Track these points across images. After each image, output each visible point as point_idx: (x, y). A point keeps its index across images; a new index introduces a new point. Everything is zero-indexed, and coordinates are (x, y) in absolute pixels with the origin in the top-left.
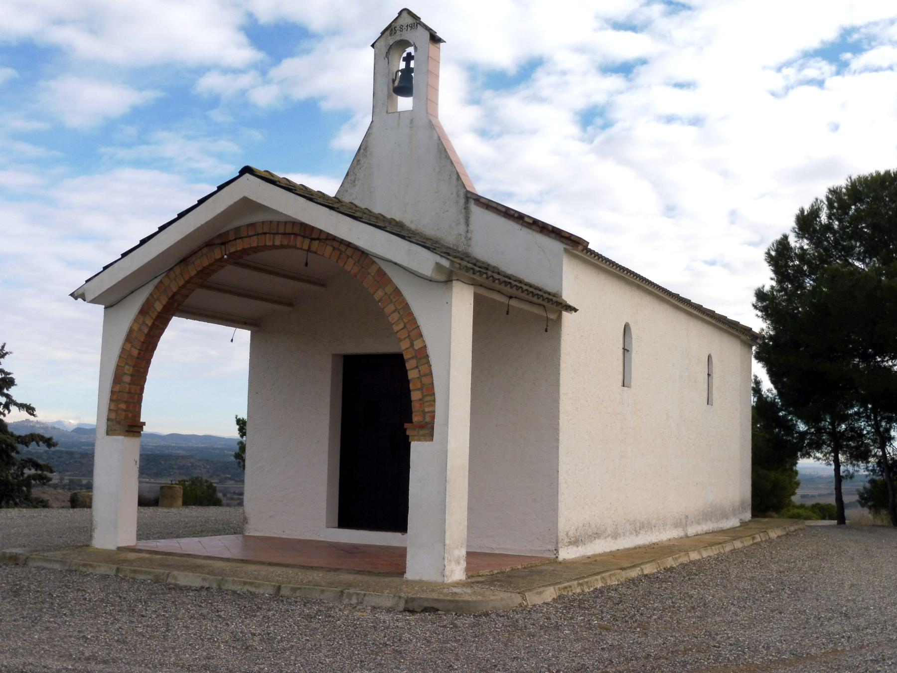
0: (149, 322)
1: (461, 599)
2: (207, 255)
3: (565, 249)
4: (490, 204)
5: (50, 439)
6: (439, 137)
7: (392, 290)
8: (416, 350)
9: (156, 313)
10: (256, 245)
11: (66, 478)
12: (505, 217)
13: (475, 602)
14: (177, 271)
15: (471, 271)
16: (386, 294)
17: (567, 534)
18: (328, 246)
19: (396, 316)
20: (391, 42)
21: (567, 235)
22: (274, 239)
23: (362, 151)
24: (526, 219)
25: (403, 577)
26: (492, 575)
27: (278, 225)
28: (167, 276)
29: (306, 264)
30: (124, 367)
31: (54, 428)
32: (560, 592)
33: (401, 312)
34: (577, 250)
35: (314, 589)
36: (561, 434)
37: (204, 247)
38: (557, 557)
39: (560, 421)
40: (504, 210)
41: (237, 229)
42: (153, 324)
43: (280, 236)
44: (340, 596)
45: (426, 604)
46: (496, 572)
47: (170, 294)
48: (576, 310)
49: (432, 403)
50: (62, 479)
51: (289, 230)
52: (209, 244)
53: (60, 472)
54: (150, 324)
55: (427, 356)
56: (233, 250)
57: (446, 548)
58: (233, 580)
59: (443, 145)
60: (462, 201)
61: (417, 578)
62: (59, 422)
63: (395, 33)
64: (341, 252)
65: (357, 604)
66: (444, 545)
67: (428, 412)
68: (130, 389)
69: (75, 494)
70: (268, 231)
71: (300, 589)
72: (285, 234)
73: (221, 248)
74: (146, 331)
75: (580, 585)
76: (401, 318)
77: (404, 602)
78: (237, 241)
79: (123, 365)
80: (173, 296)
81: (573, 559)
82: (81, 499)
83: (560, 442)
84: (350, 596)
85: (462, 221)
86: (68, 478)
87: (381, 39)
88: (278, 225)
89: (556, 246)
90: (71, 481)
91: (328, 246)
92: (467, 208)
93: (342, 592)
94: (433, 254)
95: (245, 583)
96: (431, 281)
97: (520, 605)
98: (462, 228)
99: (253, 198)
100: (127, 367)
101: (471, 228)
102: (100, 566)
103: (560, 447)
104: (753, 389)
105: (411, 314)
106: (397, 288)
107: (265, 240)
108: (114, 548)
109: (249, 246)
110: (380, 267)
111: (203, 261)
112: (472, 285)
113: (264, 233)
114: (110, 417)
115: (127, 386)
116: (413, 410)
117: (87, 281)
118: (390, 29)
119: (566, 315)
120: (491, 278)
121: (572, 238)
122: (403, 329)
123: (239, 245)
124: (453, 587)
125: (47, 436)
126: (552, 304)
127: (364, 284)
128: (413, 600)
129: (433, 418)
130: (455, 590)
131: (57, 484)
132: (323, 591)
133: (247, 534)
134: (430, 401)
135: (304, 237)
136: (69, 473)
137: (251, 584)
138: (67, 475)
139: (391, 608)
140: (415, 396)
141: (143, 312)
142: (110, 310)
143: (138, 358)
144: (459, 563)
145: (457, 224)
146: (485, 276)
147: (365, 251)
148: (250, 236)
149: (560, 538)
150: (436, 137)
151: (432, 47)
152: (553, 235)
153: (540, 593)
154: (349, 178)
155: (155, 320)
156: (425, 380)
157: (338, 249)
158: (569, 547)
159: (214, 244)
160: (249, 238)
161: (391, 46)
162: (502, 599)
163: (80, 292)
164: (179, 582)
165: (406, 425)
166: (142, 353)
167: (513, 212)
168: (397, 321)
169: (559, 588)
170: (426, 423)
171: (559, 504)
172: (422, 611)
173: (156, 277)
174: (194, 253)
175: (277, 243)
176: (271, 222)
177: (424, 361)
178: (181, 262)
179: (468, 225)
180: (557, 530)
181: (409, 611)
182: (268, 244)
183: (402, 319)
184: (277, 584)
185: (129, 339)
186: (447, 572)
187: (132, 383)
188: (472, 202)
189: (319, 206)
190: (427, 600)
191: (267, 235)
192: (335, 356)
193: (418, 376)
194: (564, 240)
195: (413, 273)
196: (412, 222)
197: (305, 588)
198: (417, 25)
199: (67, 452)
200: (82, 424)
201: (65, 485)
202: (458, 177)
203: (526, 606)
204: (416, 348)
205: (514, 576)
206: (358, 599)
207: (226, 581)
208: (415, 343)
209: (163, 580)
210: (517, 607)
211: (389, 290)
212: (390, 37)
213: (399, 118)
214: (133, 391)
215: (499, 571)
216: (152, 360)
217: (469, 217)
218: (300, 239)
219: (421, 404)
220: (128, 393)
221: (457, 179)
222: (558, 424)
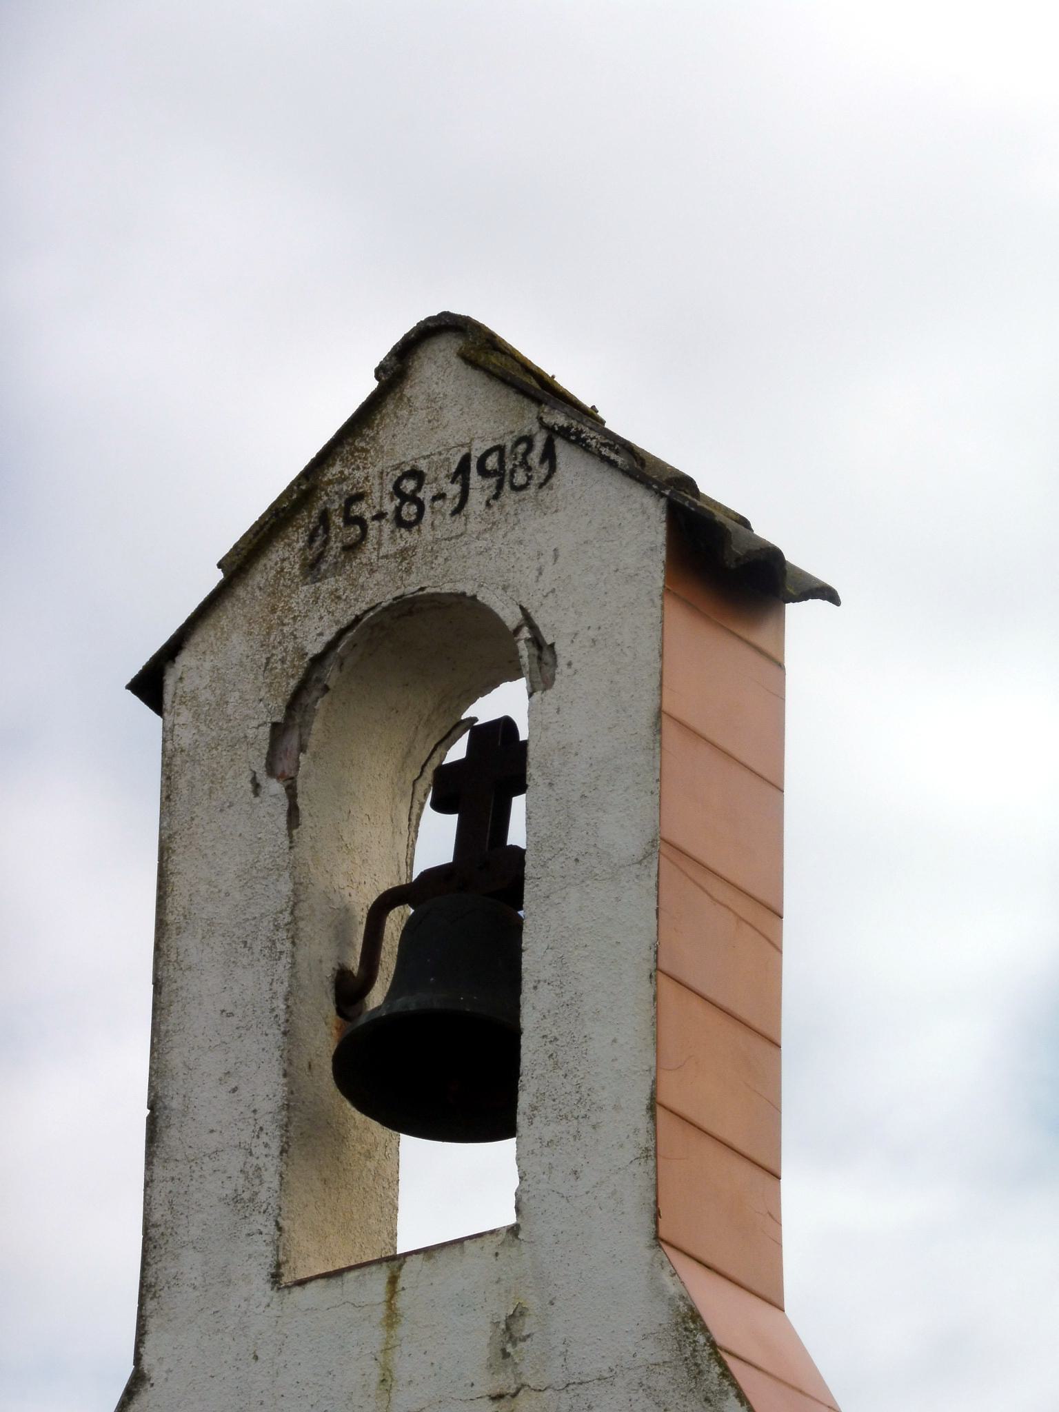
63: (351, 549)
87: (231, 614)
104: (342, 975)
161: (318, 660)
195: (758, 901)
198: (549, 455)
212: (305, 590)
213: (392, 1317)
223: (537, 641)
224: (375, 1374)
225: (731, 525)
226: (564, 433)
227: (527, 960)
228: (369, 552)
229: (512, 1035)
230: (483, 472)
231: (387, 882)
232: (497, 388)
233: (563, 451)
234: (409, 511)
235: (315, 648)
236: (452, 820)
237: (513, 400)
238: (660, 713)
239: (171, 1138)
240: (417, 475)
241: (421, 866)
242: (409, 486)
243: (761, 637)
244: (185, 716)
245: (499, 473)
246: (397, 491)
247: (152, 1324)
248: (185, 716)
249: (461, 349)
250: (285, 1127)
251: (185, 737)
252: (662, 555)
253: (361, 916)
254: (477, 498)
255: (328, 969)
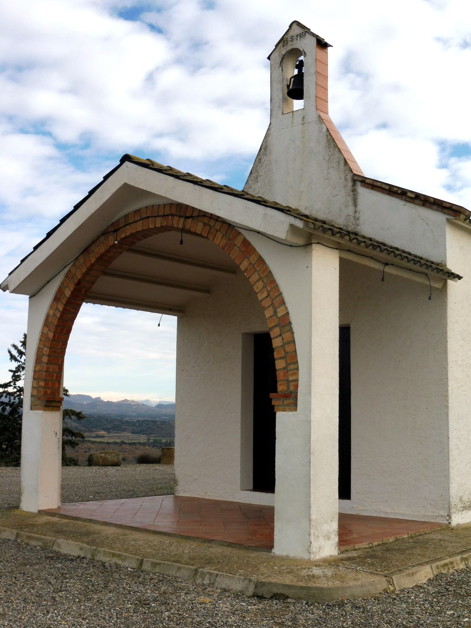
0: (61, 308)
1: (314, 585)
2: (103, 243)
3: (447, 219)
4: (375, 183)
5: (80, 413)
6: (327, 129)
7: (256, 259)
8: (279, 318)
9: (66, 299)
10: (141, 229)
11: (151, 438)
12: (388, 194)
13: (329, 589)
14: (81, 260)
15: (330, 232)
16: (251, 263)
17: (461, 499)
18: (199, 223)
19: (260, 285)
20: (284, 53)
21: (448, 205)
22: (155, 221)
23: (262, 150)
24: (409, 194)
25: (271, 552)
26: (370, 548)
27: (158, 208)
28: (74, 265)
29: (181, 242)
30: (43, 349)
31: (143, 405)
32: (438, 570)
33: (265, 281)
34: (459, 220)
35: (172, 565)
36: (450, 401)
37: (101, 236)
38: (450, 523)
39: (450, 388)
40: (387, 188)
41: (127, 216)
42: (64, 309)
43: (160, 218)
44: (194, 575)
45: (275, 590)
46: (376, 543)
47: (76, 281)
48: (460, 278)
49: (295, 371)
50: (149, 440)
51: (167, 212)
52: (105, 233)
53: (148, 435)
54: (61, 310)
55: (290, 323)
56: (123, 236)
57: (313, 523)
58: (105, 551)
59: (331, 135)
60: (350, 184)
61: (284, 554)
62: (147, 401)
63: (287, 44)
64: (211, 226)
65: (209, 585)
66: (310, 520)
67: (292, 381)
68: (48, 368)
69: (91, 455)
70: (151, 215)
71: (159, 564)
72: (164, 216)
73: (114, 235)
74: (58, 315)
75: (463, 559)
76: (265, 287)
77: (254, 587)
78: (127, 227)
79: (42, 347)
80: (79, 283)
81: (468, 523)
82: (95, 459)
83: (450, 408)
84: (203, 575)
85: (351, 203)
86: (153, 438)
87: (276, 50)
88: (158, 208)
89: (439, 217)
90: (154, 440)
91: (199, 223)
92: (354, 191)
93: (196, 570)
94: (288, 216)
95: (114, 555)
96: (291, 246)
97: (385, 591)
98: (351, 210)
99: (131, 183)
100: (45, 349)
101: (359, 208)
102: (5, 531)
103: (450, 415)
105: (273, 281)
106: (260, 256)
107: (148, 222)
108: (35, 511)
109: (135, 231)
110: (245, 238)
111: (100, 249)
112: (337, 249)
113: (148, 217)
114: (33, 394)
115: (45, 365)
116: (278, 380)
117: (10, 274)
118: (283, 41)
119: (450, 282)
120: (355, 241)
121: (454, 207)
122: (266, 297)
123: (128, 231)
124: (316, 566)
125: (78, 410)
126: (432, 271)
127: (231, 255)
128: (263, 584)
129: (297, 387)
130: (316, 571)
131: (145, 443)
132: (179, 569)
133: (177, 495)
134: (294, 369)
135: (180, 217)
136: (153, 435)
137: (119, 556)
138: (152, 437)
139: (240, 592)
140: (280, 364)
141: (56, 299)
142: (34, 298)
143: (53, 340)
144: (329, 538)
145: (346, 206)
146: (347, 238)
147: (232, 223)
148: (136, 222)
149: (453, 504)
150: (324, 130)
151: (320, 52)
152: (435, 207)
153: (413, 574)
154: (253, 175)
155: (65, 305)
156: (289, 348)
157: (209, 225)
158: (463, 512)
159: (108, 233)
160: (135, 223)
161: (284, 55)
162: (362, 586)
163: (5, 284)
164: (61, 550)
165: (272, 395)
166: (57, 335)
167: (396, 189)
168: (260, 290)
169: (437, 566)
170: (290, 392)
171: (451, 470)
172: (271, 598)
173: (65, 267)
174: (94, 242)
175: (158, 225)
176: (153, 206)
177: (287, 328)
178: (84, 251)
179: (355, 204)
180: (449, 496)
181: (258, 597)
182: (150, 227)
183: (266, 288)
184: (141, 558)
185: (46, 323)
186: (314, 548)
187: (49, 362)
188: (359, 184)
189: (185, 182)
190: (276, 585)
191: (150, 218)
192: (246, 335)
193: (282, 344)
194: (446, 211)
196: (306, 208)
197: (164, 564)
198: (305, 34)
199: (152, 421)
200: (162, 401)
201: (150, 444)
202: (346, 163)
203: (393, 592)
204: (279, 315)
205: (394, 549)
206: (210, 580)
207: (99, 552)
208: (278, 310)
209: (49, 547)
210: (380, 593)
211: (253, 259)
212: (283, 48)
214: (51, 370)
215: (381, 543)
216: (68, 342)
217: (357, 199)
218: (176, 218)
219: (285, 373)
220: (46, 372)
221: (345, 165)
222: (448, 390)
223: (304, 52)
224: (291, 122)
225: (322, 40)
226: (306, 32)
227: (304, 83)
228: (288, 44)
229: (303, 90)
230: (299, 36)
231: (291, 76)
232: (300, 28)
233: (306, 33)
234: (292, 40)
235: (284, 54)
236: (297, 70)
237: (301, 29)
238: (316, 59)
239: (272, 101)
240: (293, 36)
241: (294, 74)
242: (292, 37)
243: (325, 51)
244: (272, 61)
245: (300, 36)
246: (291, 38)
247: (272, 118)
248: (272, 61)
249: (288, 86)
250: (283, 100)
251: (272, 63)
252: (316, 43)
253: (289, 79)
254: (298, 38)
255: (286, 84)
